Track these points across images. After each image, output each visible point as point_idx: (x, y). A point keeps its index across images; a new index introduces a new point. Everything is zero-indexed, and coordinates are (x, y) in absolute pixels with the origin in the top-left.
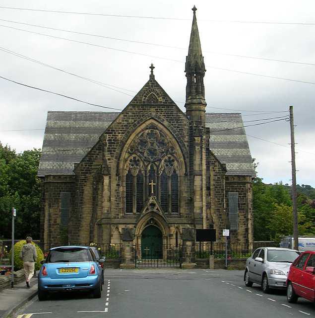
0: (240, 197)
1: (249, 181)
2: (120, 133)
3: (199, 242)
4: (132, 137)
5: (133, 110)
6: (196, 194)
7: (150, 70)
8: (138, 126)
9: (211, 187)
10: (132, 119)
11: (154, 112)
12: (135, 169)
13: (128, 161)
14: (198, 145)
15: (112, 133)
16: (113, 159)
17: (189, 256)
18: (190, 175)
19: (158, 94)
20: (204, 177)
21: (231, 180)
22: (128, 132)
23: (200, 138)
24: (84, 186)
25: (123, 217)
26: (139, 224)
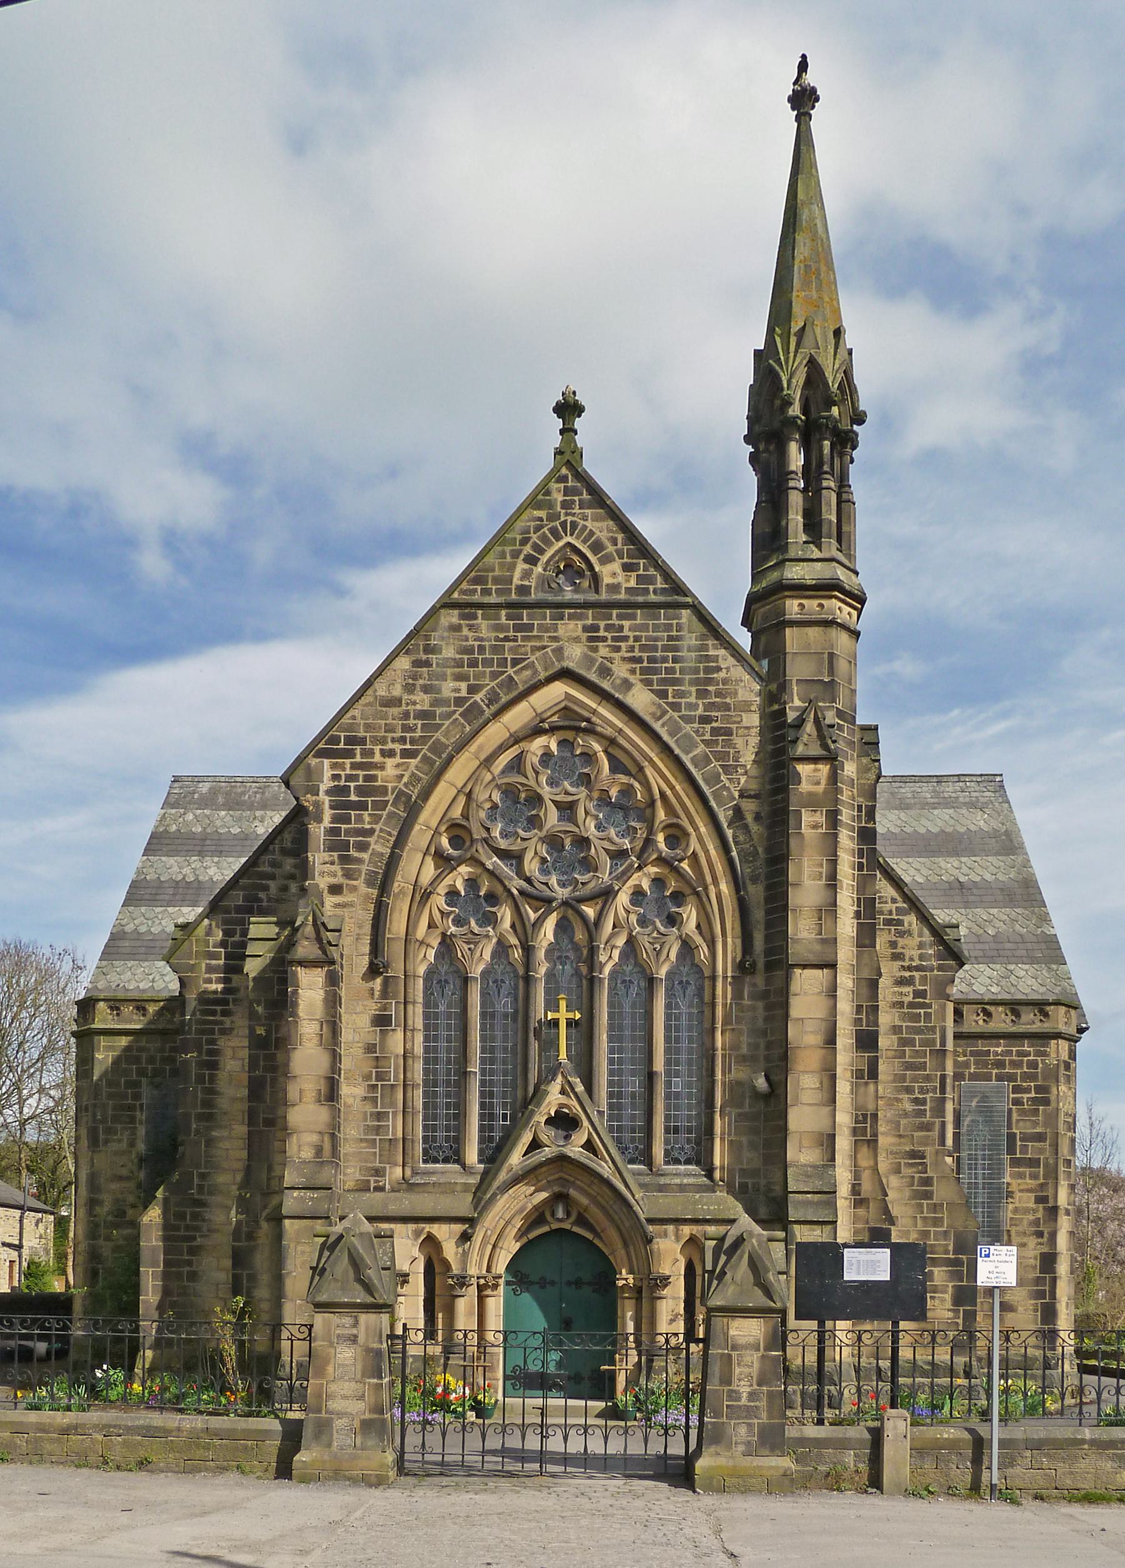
0: (1017, 1102)
1: (1062, 1028)
2: (391, 754)
3: (813, 1325)
4: (459, 772)
5: (465, 631)
6: (800, 1067)
7: (559, 423)
8: (488, 712)
9: (883, 1042)
10: (459, 678)
11: (577, 640)
12: (473, 939)
13: (439, 900)
14: (812, 802)
15: (350, 754)
16: (354, 889)
17: (750, 1412)
18: (770, 967)
19: (597, 547)
20: (845, 981)
21: (974, 1022)
22: (437, 748)
23: (824, 769)
24: (223, 1032)
25: (407, 1185)
26: (491, 1220)
